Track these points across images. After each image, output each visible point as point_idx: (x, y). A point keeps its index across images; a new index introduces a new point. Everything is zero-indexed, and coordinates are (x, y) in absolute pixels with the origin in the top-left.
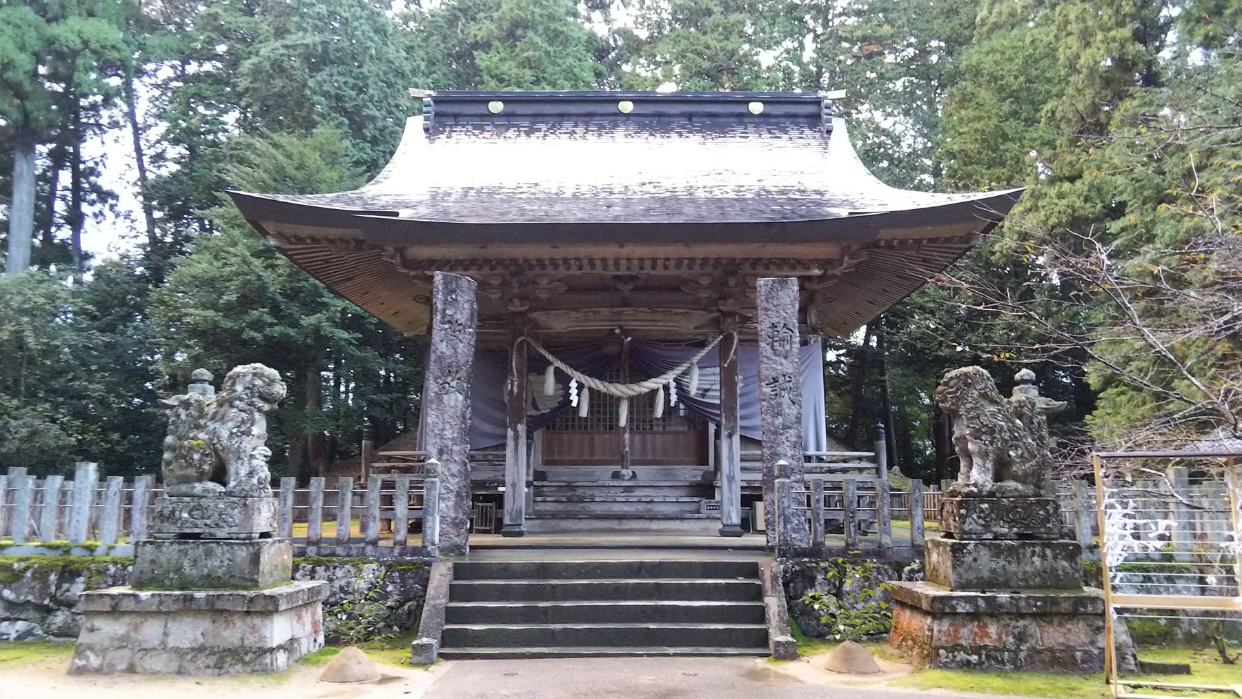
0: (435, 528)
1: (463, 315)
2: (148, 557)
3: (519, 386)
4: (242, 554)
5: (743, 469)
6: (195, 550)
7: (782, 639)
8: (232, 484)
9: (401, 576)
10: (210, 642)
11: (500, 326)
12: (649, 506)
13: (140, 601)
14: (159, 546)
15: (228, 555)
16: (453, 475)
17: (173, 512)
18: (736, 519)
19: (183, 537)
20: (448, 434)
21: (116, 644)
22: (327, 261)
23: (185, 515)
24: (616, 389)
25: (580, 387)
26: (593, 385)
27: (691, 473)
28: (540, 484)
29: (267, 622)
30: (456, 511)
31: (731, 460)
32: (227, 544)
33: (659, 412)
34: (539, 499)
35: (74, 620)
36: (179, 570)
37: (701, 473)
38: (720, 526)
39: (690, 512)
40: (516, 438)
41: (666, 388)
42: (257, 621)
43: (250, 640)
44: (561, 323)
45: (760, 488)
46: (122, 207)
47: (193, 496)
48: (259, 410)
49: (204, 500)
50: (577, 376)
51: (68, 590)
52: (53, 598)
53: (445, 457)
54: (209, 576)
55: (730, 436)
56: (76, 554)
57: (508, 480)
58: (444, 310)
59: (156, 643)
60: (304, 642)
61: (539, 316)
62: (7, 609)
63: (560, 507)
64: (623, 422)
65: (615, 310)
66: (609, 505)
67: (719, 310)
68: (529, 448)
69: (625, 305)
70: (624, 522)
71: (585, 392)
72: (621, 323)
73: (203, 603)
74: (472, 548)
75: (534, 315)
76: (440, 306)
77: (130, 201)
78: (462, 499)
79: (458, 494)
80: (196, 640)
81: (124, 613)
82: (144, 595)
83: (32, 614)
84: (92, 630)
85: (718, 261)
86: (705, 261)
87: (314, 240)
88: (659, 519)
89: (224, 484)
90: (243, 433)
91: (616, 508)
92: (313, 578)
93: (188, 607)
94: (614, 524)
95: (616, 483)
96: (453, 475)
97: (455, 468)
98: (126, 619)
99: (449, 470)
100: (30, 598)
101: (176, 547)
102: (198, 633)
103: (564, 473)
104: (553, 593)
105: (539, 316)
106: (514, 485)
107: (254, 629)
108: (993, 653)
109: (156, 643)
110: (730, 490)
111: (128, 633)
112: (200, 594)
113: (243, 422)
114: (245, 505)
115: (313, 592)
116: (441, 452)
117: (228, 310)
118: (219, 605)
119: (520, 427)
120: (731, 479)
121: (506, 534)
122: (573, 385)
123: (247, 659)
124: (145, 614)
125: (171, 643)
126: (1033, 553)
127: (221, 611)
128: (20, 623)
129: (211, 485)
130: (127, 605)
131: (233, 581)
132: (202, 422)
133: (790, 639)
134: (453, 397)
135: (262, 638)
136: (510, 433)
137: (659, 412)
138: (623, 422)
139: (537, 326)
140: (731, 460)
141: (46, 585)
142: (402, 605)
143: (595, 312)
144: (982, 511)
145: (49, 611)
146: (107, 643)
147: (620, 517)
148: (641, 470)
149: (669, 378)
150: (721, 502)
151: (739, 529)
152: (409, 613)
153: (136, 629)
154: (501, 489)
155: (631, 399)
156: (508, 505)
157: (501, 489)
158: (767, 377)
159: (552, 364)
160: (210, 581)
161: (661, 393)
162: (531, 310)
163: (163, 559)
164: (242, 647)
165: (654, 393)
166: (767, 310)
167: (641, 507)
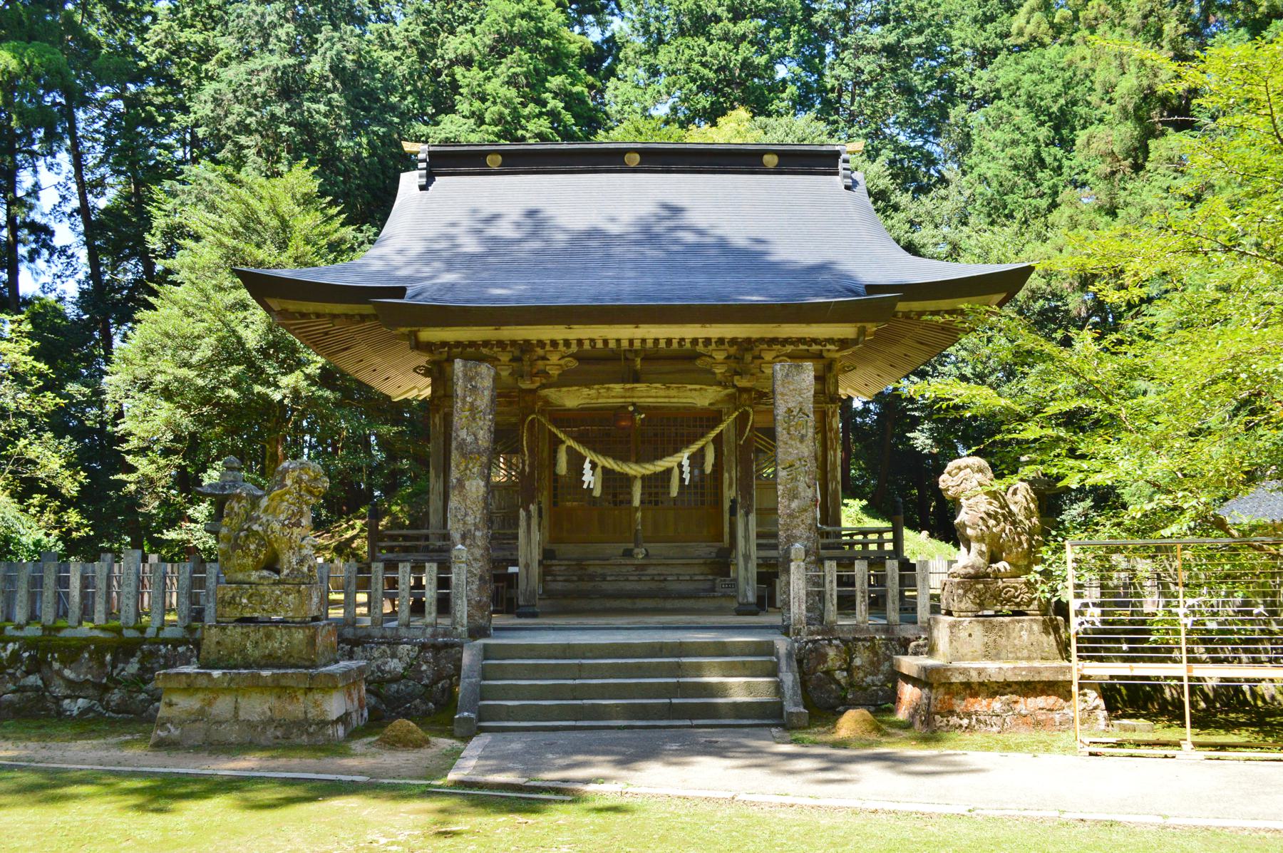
0: (462, 609)
1: (484, 401)
2: (215, 639)
3: (531, 466)
4: (299, 635)
5: (759, 546)
6: (257, 634)
7: (794, 710)
8: (286, 572)
9: (435, 657)
10: (277, 716)
11: (510, 403)
12: (663, 585)
13: (213, 679)
14: (224, 629)
15: (286, 637)
16: (475, 559)
17: (233, 597)
18: (751, 598)
19: (243, 621)
20: (470, 519)
21: (193, 717)
22: (326, 334)
23: (244, 601)
24: (633, 469)
25: (594, 466)
26: (607, 465)
27: (705, 550)
28: (549, 562)
29: (327, 697)
30: (480, 595)
31: (747, 538)
32: (286, 628)
33: (674, 491)
34: (549, 578)
35: (131, 697)
36: (243, 650)
37: (715, 550)
38: (736, 605)
39: (704, 590)
40: (529, 517)
41: (680, 466)
42: (318, 696)
43: (312, 714)
44: (572, 399)
45: (776, 565)
46: (57, 242)
47: (250, 583)
48: (307, 504)
49: (260, 587)
50: (590, 456)
51: (123, 670)
52: (110, 677)
53: (468, 542)
54: (270, 655)
55: (747, 514)
56: (130, 634)
57: (521, 560)
58: (465, 397)
59: (229, 716)
60: (354, 715)
61: (552, 394)
62: (68, 687)
63: (570, 586)
64: (637, 502)
65: (628, 386)
66: (621, 584)
67: (734, 386)
68: (539, 524)
69: (637, 381)
70: (638, 601)
71: (599, 470)
72: (635, 400)
73: (270, 680)
74: (495, 629)
75: (545, 392)
76: (459, 392)
77: (66, 234)
78: (485, 582)
79: (481, 578)
80: (264, 713)
81: (197, 690)
82: (216, 673)
83: (91, 692)
84: (170, 705)
85: (733, 341)
86: (721, 341)
87: (318, 315)
88: (674, 598)
89: (278, 572)
90: (294, 525)
91: (629, 586)
92: (351, 658)
93: (258, 685)
94: (627, 604)
95: (628, 562)
96: (475, 559)
97: (478, 552)
98: (201, 695)
99: (472, 554)
100: (89, 677)
101: (239, 630)
102: (266, 707)
103: (570, 550)
104: (580, 671)
105: (552, 394)
106: (527, 566)
107: (316, 704)
108: (982, 718)
109: (229, 716)
110: (746, 569)
111: (202, 708)
112: (266, 673)
113: (293, 514)
114: (299, 591)
115: (361, 670)
116: (464, 537)
117: (203, 367)
118: (284, 682)
119: (532, 507)
120: (747, 557)
121: (520, 616)
122: (587, 466)
123: (311, 730)
124: (216, 689)
125: (242, 716)
126: (1022, 629)
127: (286, 688)
128: (80, 700)
129: (265, 573)
130: (203, 682)
131: (292, 661)
132: (254, 514)
133: (802, 710)
134: (474, 483)
135: (324, 712)
136: (522, 513)
137: (674, 491)
138: (637, 502)
139: (547, 402)
140: (747, 538)
141: (102, 664)
142: (437, 683)
143: (608, 389)
144: (978, 591)
145: (106, 689)
146: (184, 716)
147: (633, 596)
148: (654, 548)
149: (684, 457)
150: (736, 580)
151: (754, 608)
152: (444, 690)
153: (210, 704)
154: (512, 570)
155: (643, 478)
156: (522, 585)
157: (512, 570)
158: (783, 461)
159: (563, 442)
160: (271, 661)
161: (676, 471)
162: (544, 386)
163: (228, 641)
164: (306, 719)
165: (669, 471)
166: (783, 394)
167: (654, 585)
